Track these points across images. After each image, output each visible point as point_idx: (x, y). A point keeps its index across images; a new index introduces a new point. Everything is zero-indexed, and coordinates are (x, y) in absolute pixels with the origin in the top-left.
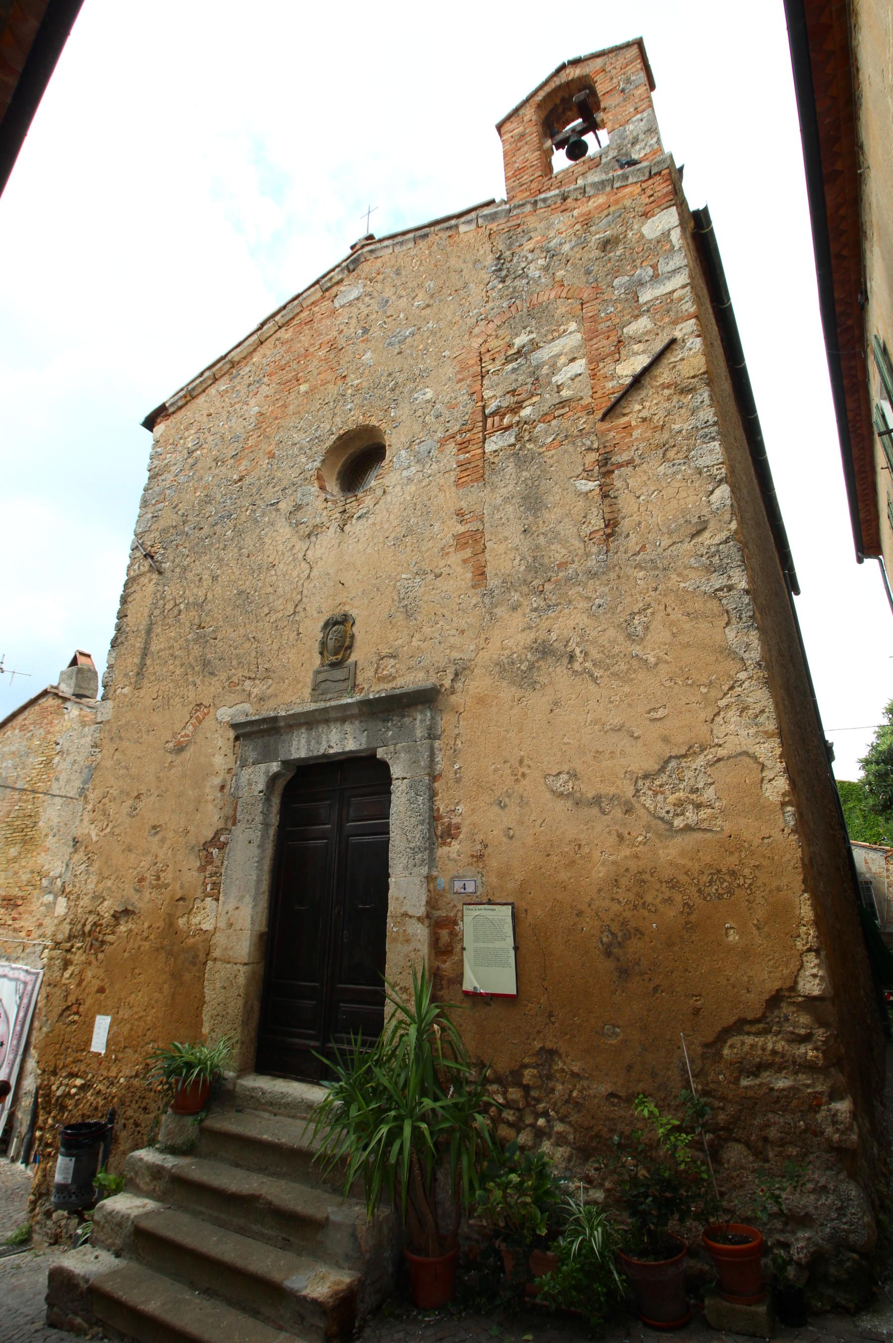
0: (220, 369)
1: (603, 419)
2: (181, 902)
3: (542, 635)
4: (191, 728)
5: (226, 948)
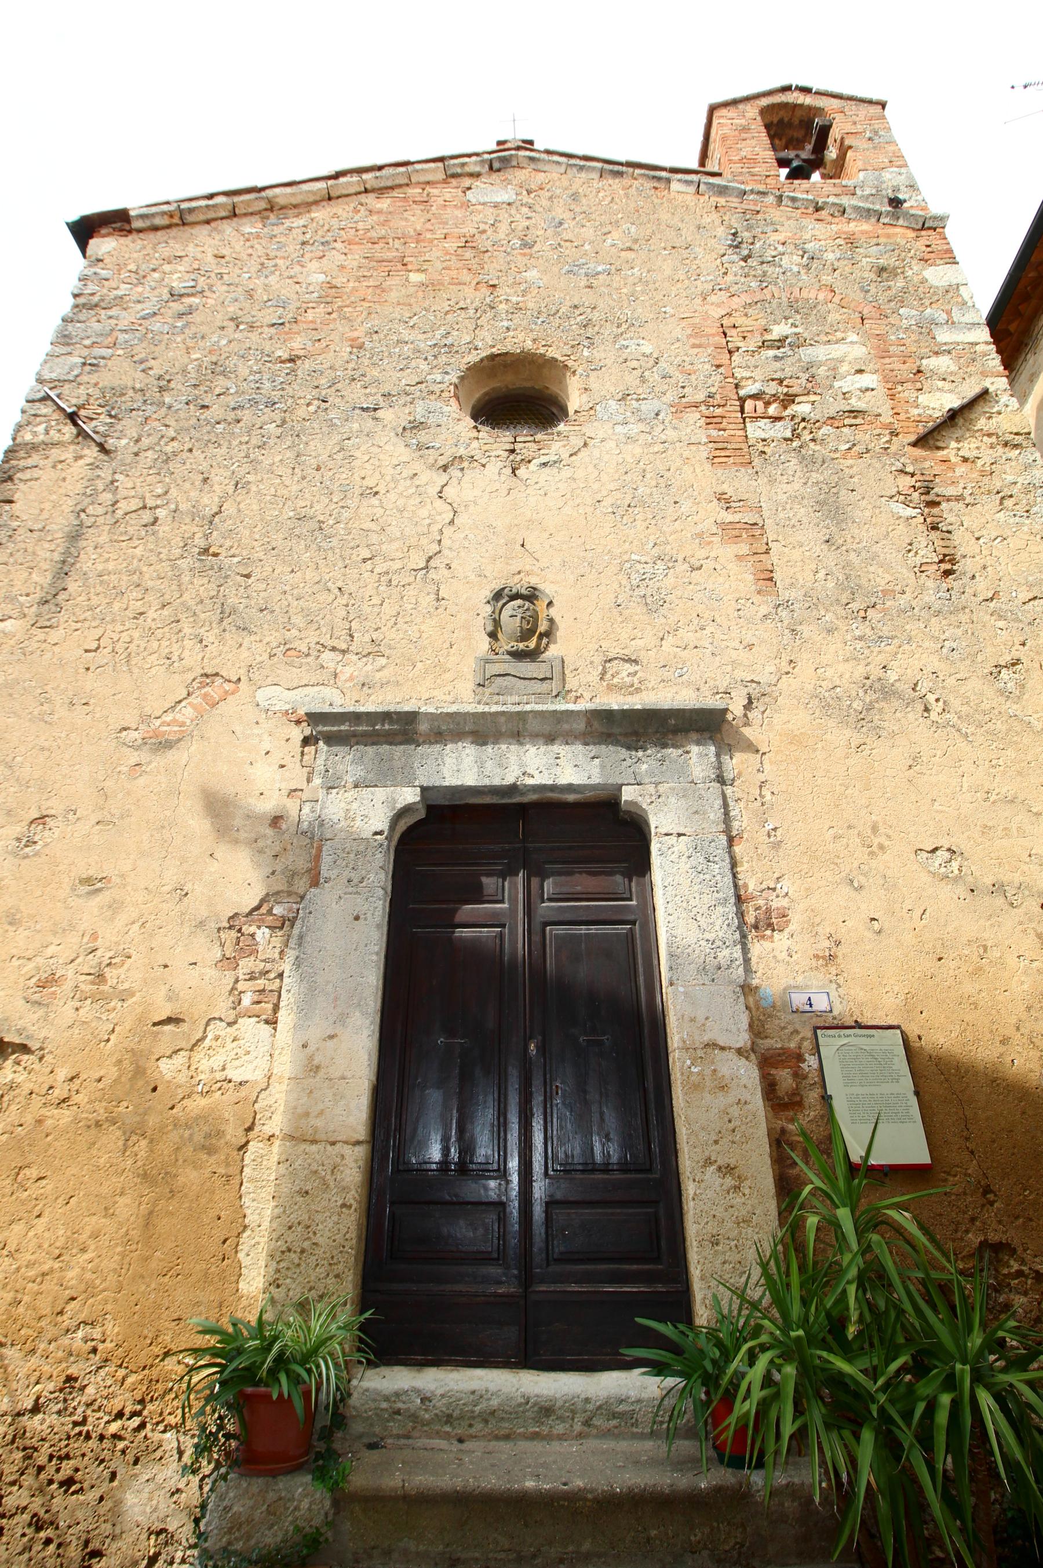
0: (248, 203)
1: (915, 444)
2: (167, 1028)
3: (876, 672)
4: (189, 712)
5: (307, 1114)
